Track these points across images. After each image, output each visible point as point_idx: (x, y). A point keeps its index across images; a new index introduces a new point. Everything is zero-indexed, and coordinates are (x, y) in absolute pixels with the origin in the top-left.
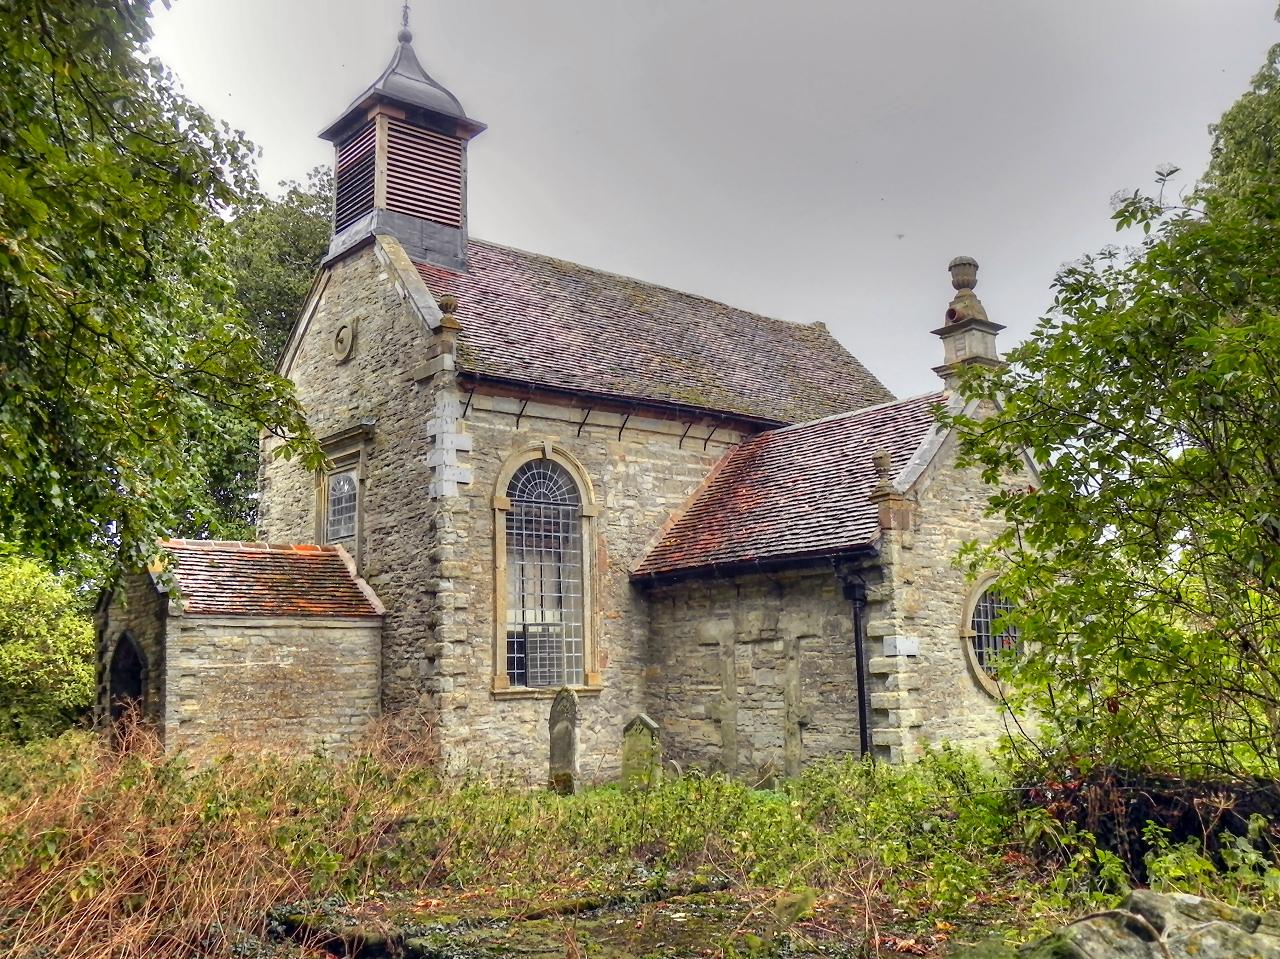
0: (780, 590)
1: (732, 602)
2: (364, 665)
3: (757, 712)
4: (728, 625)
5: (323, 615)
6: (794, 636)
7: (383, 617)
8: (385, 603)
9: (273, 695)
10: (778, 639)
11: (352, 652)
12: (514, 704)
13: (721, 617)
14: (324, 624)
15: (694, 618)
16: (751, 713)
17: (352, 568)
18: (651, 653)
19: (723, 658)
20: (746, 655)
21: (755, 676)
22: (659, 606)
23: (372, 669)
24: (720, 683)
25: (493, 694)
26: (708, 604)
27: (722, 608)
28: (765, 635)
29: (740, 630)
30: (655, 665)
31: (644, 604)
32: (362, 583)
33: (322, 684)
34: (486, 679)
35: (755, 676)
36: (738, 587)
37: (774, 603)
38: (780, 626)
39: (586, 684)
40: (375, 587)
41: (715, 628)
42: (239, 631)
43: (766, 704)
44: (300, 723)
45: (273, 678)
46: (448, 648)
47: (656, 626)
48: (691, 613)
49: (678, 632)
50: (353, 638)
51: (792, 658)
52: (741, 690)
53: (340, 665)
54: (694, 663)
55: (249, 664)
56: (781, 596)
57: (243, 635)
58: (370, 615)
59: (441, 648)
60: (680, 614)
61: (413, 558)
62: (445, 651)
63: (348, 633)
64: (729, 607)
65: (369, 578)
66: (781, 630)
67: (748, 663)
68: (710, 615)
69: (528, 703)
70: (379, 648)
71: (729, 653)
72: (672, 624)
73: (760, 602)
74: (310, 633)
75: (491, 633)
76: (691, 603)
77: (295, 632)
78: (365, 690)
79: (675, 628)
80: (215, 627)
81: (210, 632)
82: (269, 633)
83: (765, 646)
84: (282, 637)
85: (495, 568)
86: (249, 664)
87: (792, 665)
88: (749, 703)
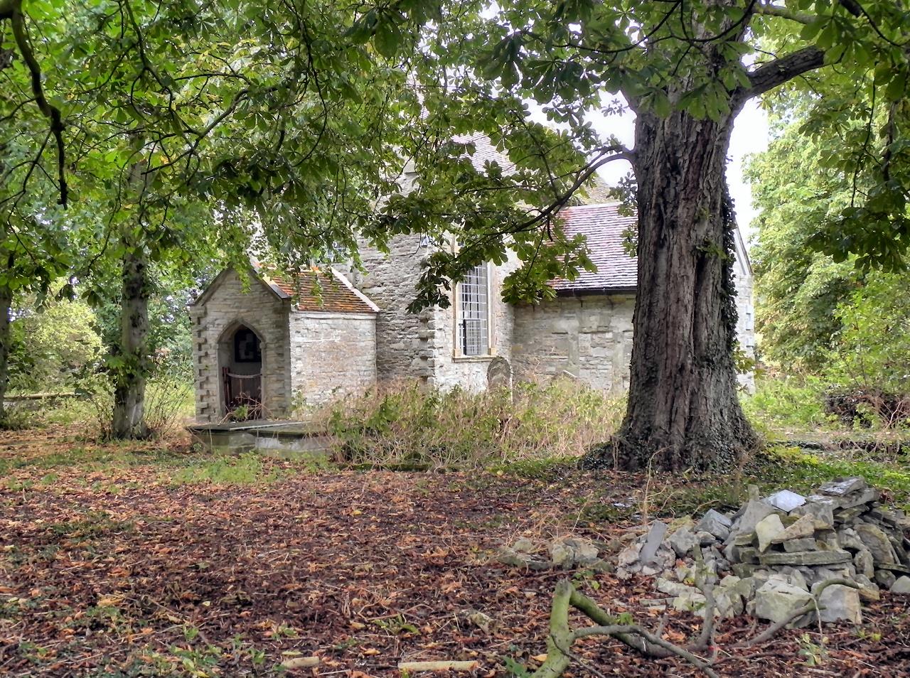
0: (612, 305)
1: (577, 310)
2: (367, 342)
3: (593, 371)
4: (575, 323)
5: (353, 312)
6: (621, 331)
7: (378, 313)
8: (378, 305)
9: (333, 359)
10: (608, 332)
11: (364, 334)
12: (461, 365)
13: (568, 318)
14: (323, 316)
15: (549, 318)
16: (589, 371)
17: (349, 285)
18: (517, 336)
19: (571, 341)
20: (586, 340)
21: (592, 351)
22: (522, 310)
23: (372, 344)
24: (568, 355)
25: (454, 359)
26: (559, 310)
27: (570, 313)
28: (600, 329)
29: (583, 325)
30: (519, 344)
31: (512, 309)
32: (357, 292)
33: (352, 353)
34: (451, 350)
35: (592, 351)
36: (582, 302)
37: (607, 312)
38: (611, 324)
39: (489, 353)
40: (369, 295)
41: (564, 324)
42: (317, 321)
43: (599, 367)
44: (344, 375)
45: (333, 348)
46: (438, 334)
47: (519, 321)
48: (546, 315)
49: (536, 326)
50: (364, 325)
51: (619, 342)
52: (582, 359)
53: (360, 341)
54: (548, 343)
55: (323, 340)
56: (612, 308)
57: (319, 324)
58: (372, 312)
59: (434, 333)
60: (538, 315)
61: (404, 280)
62: (436, 335)
63: (363, 322)
64: (574, 313)
65: (362, 289)
66: (612, 327)
67: (588, 344)
68: (561, 316)
69: (466, 364)
70: (375, 331)
71: (575, 338)
72: (532, 321)
73: (597, 311)
74: (346, 322)
75: (452, 324)
76: (546, 309)
77: (341, 321)
78: (370, 356)
79: (534, 323)
80: (308, 318)
81: (306, 321)
82: (330, 322)
83: (600, 335)
84: (335, 325)
85: (696, 314)
86: (323, 340)
87: (619, 346)
88: (588, 366)
